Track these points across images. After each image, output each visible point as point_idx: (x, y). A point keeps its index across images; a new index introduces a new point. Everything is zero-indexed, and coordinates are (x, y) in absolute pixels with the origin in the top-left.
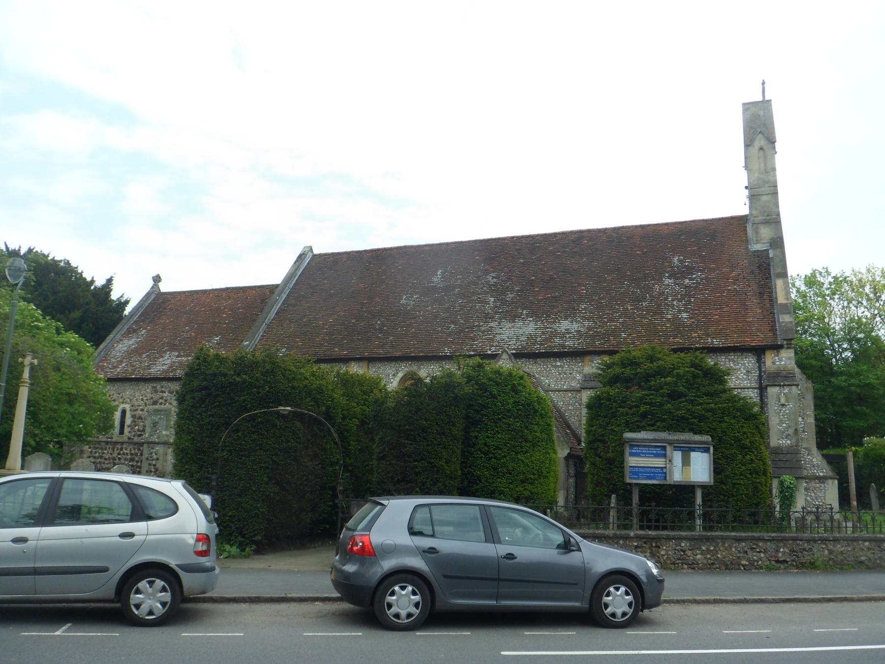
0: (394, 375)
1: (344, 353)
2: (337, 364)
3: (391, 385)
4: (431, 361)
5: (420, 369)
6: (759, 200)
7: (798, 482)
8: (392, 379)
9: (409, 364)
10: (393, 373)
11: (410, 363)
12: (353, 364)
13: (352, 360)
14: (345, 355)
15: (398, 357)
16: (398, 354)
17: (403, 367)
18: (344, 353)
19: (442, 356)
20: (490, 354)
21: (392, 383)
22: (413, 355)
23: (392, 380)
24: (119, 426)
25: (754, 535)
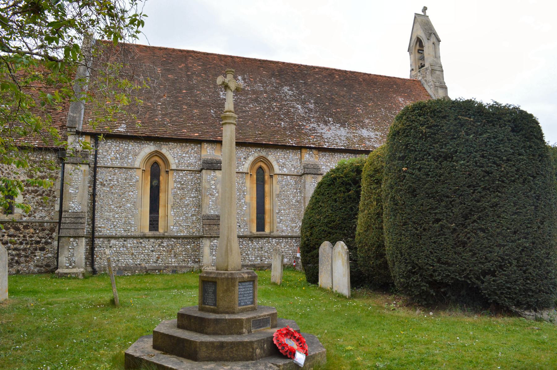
0: (245, 158)
1: (195, 134)
2: (188, 144)
3: (243, 167)
4: (277, 149)
5: (267, 154)
6: (435, 73)
7: (61, 267)
8: (244, 161)
9: (258, 150)
10: (244, 156)
11: (259, 149)
12: (206, 145)
13: (205, 142)
14: (197, 136)
15: (249, 143)
16: (251, 141)
17: (253, 152)
18: (195, 134)
19: (290, 146)
20: (325, 148)
21: (243, 165)
22: (264, 142)
23: (244, 163)
24: (153, 232)
25: (343, 132)
